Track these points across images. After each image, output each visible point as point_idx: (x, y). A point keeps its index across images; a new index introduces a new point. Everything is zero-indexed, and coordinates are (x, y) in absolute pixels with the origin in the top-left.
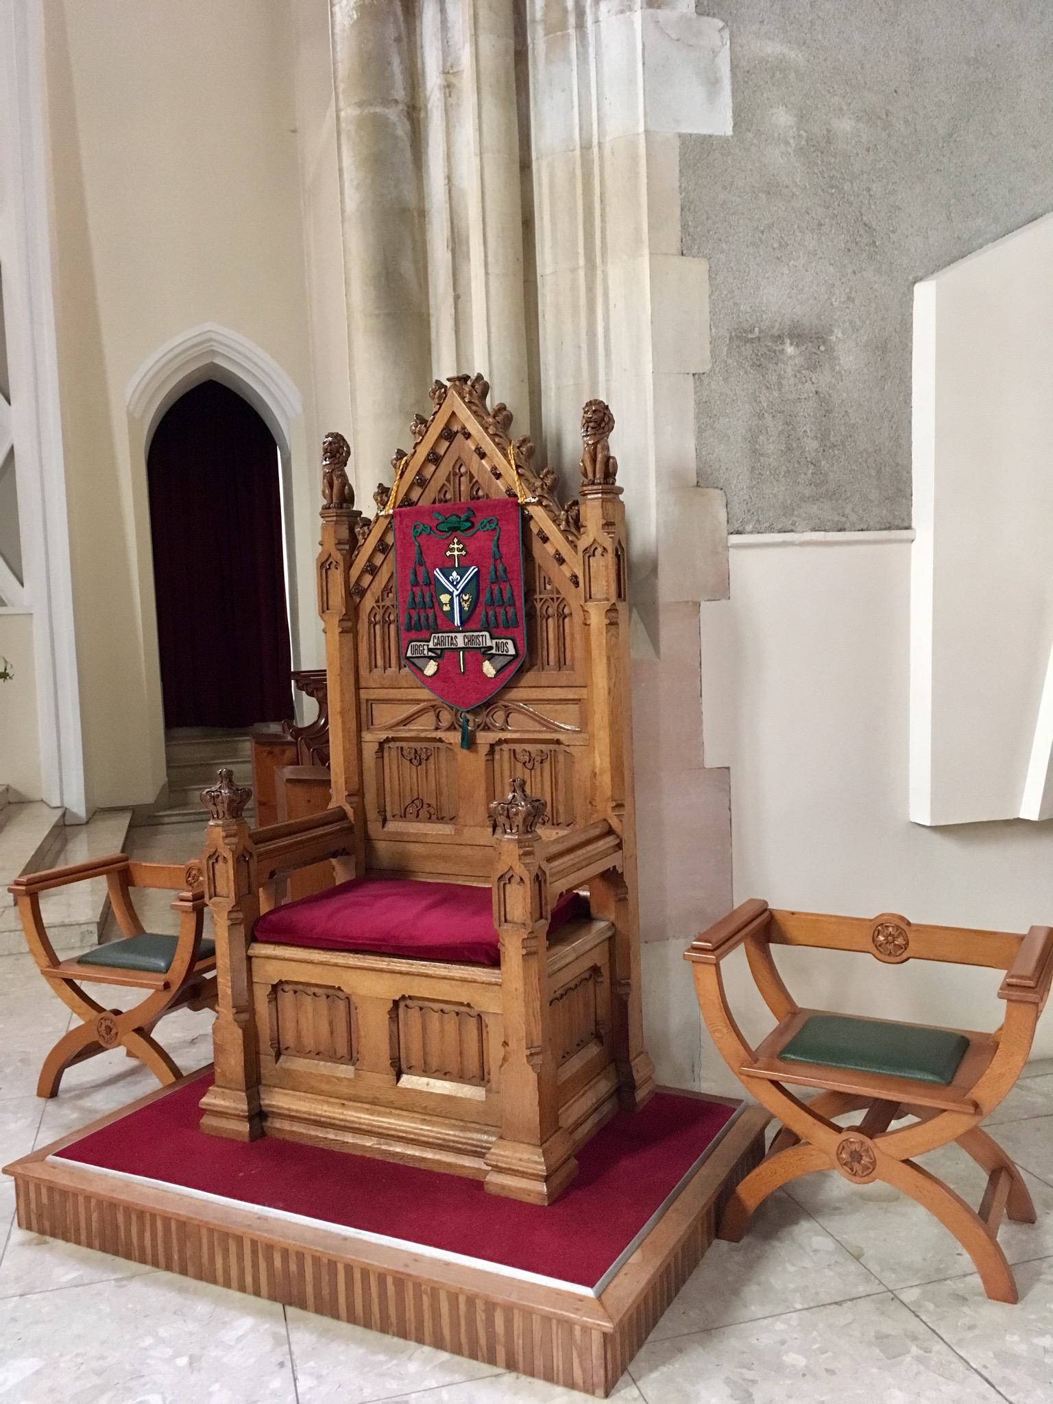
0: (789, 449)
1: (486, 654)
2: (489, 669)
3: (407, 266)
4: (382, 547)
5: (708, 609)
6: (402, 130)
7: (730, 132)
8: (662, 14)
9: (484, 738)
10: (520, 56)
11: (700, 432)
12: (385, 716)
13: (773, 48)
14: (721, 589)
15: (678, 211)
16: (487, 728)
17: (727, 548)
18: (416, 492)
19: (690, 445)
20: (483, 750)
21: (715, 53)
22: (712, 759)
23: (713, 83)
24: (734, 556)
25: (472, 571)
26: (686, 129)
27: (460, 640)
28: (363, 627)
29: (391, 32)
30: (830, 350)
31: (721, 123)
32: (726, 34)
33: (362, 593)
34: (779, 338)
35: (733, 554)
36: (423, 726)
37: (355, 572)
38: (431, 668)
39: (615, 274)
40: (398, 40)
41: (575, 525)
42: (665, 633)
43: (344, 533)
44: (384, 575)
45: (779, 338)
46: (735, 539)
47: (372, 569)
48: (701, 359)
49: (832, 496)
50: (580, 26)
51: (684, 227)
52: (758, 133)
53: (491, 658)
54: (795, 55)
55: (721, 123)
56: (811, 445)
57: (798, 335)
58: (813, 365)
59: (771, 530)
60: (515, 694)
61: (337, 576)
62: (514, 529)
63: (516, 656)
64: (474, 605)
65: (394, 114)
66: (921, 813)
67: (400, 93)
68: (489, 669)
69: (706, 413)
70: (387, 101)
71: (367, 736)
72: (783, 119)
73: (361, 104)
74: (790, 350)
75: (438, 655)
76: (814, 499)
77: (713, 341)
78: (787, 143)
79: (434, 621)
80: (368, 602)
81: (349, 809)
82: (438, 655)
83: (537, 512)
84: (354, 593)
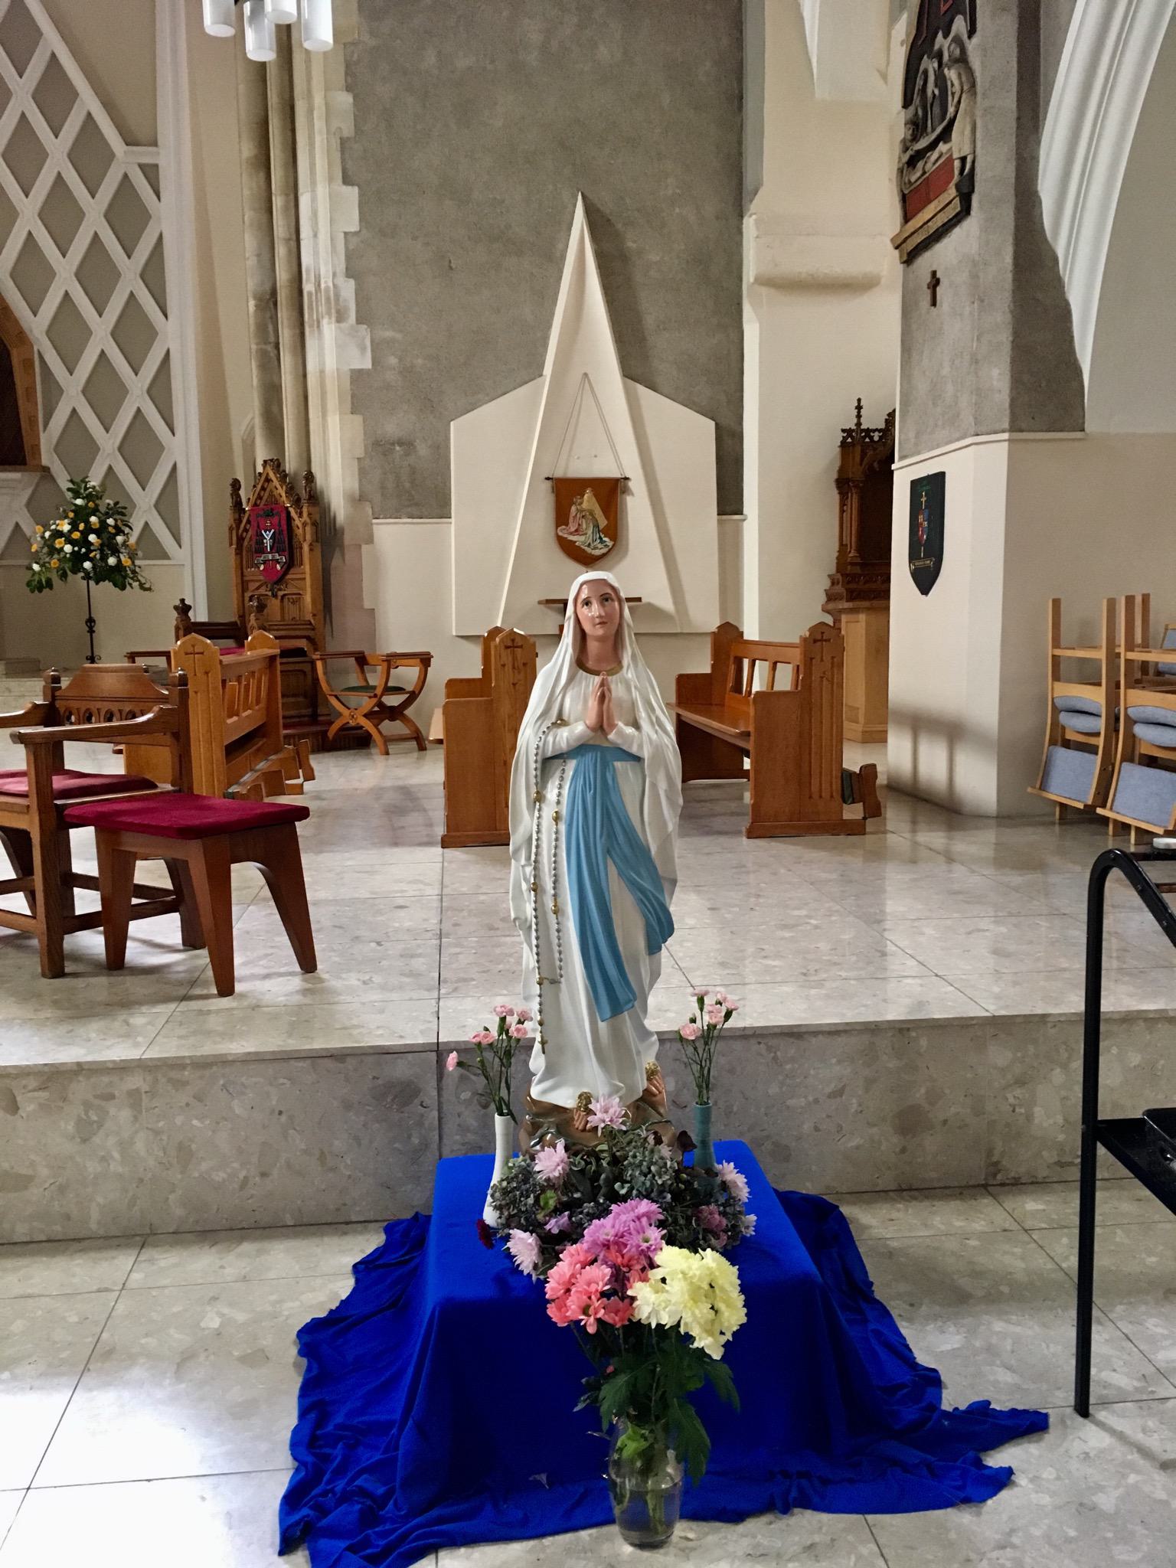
0: (398, 486)
1: (277, 561)
2: (278, 567)
3: (275, 409)
4: (248, 522)
5: (365, 548)
6: (273, 354)
7: (370, 367)
8: (343, 325)
9: (281, 593)
10: (302, 335)
11: (360, 480)
12: (252, 586)
13: (389, 334)
14: (370, 539)
15: (350, 398)
16: (280, 590)
17: (372, 524)
18: (258, 502)
19: (356, 486)
20: (280, 598)
21: (364, 338)
22: (367, 605)
23: (363, 349)
24: (375, 527)
25: (273, 531)
26: (352, 367)
27: (270, 557)
28: (244, 553)
29: (268, 315)
30: (415, 447)
31: (367, 364)
32: (369, 330)
33: (243, 539)
34: (393, 444)
35: (375, 527)
36: (262, 591)
37: (240, 531)
38: (262, 568)
39: (329, 419)
40: (271, 318)
41: (300, 515)
42: (347, 557)
43: (237, 516)
44: (250, 533)
45: (393, 444)
46: (374, 521)
47: (246, 530)
48: (360, 452)
49: (417, 504)
50: (318, 327)
51: (353, 403)
52: (382, 367)
53: (279, 563)
54: (399, 336)
55: (367, 364)
56: (407, 485)
57: (400, 443)
58: (407, 454)
59: (390, 518)
60: (288, 577)
61: (234, 532)
62: (284, 515)
63: (285, 563)
64: (273, 544)
65: (270, 348)
66: (454, 634)
67: (272, 339)
68: (278, 567)
69: (363, 472)
70: (266, 342)
71: (246, 594)
72: (393, 361)
73: (257, 344)
74: (398, 448)
75: (265, 562)
76: (409, 506)
77: (365, 446)
78: (394, 369)
79: (261, 549)
80: (246, 543)
81: (239, 622)
82: (265, 562)
83: (291, 509)
84: (240, 539)
